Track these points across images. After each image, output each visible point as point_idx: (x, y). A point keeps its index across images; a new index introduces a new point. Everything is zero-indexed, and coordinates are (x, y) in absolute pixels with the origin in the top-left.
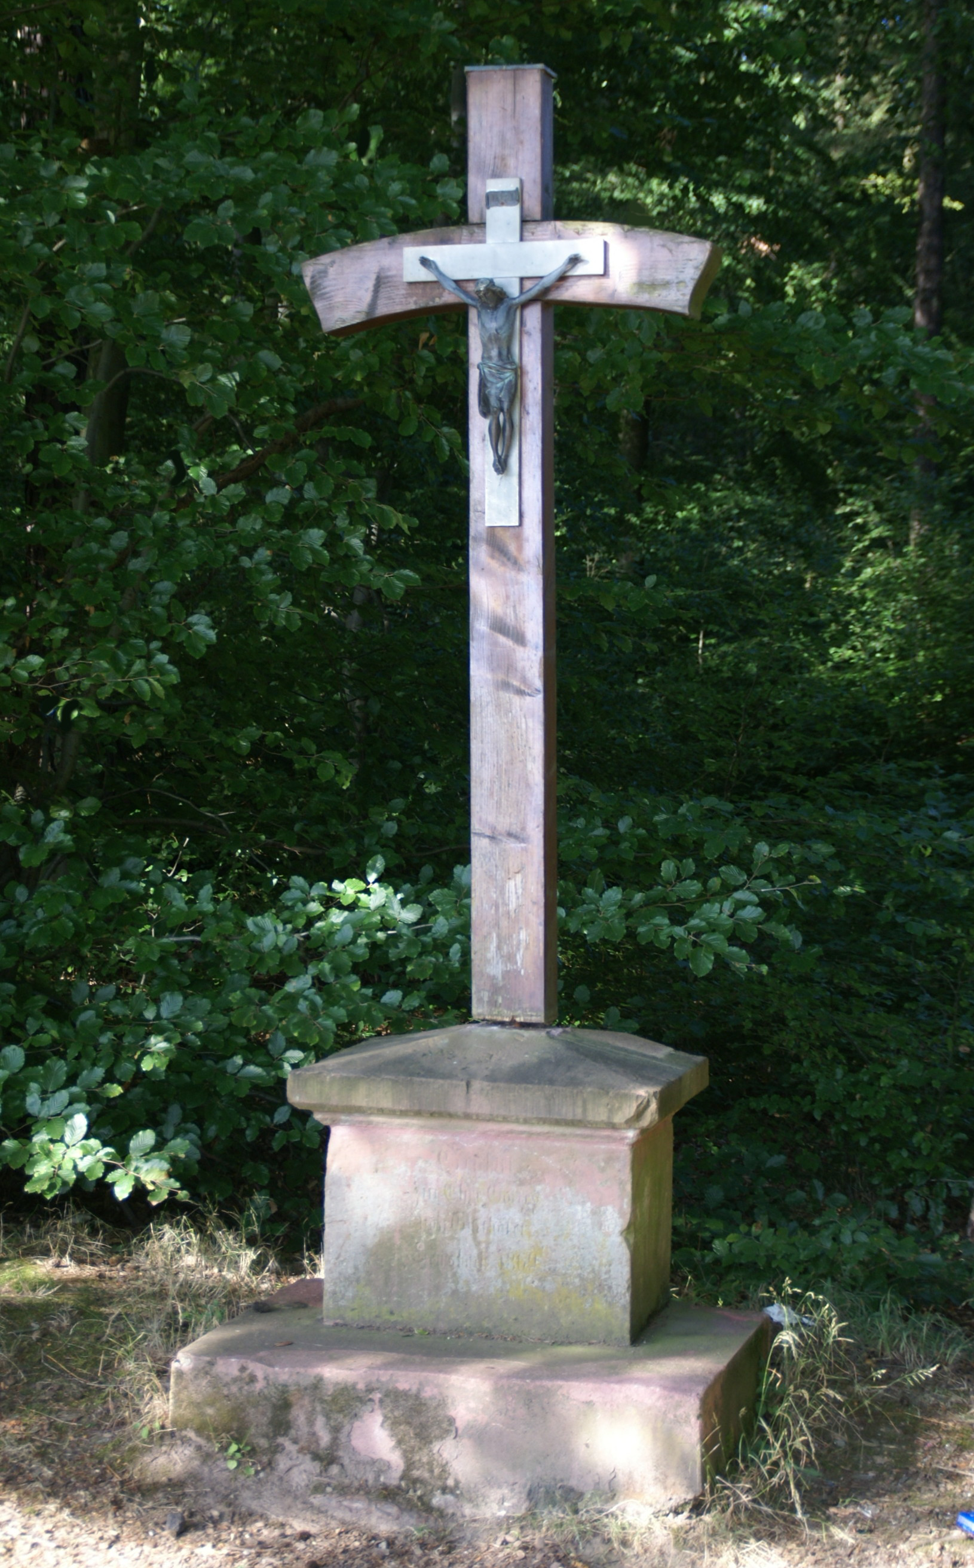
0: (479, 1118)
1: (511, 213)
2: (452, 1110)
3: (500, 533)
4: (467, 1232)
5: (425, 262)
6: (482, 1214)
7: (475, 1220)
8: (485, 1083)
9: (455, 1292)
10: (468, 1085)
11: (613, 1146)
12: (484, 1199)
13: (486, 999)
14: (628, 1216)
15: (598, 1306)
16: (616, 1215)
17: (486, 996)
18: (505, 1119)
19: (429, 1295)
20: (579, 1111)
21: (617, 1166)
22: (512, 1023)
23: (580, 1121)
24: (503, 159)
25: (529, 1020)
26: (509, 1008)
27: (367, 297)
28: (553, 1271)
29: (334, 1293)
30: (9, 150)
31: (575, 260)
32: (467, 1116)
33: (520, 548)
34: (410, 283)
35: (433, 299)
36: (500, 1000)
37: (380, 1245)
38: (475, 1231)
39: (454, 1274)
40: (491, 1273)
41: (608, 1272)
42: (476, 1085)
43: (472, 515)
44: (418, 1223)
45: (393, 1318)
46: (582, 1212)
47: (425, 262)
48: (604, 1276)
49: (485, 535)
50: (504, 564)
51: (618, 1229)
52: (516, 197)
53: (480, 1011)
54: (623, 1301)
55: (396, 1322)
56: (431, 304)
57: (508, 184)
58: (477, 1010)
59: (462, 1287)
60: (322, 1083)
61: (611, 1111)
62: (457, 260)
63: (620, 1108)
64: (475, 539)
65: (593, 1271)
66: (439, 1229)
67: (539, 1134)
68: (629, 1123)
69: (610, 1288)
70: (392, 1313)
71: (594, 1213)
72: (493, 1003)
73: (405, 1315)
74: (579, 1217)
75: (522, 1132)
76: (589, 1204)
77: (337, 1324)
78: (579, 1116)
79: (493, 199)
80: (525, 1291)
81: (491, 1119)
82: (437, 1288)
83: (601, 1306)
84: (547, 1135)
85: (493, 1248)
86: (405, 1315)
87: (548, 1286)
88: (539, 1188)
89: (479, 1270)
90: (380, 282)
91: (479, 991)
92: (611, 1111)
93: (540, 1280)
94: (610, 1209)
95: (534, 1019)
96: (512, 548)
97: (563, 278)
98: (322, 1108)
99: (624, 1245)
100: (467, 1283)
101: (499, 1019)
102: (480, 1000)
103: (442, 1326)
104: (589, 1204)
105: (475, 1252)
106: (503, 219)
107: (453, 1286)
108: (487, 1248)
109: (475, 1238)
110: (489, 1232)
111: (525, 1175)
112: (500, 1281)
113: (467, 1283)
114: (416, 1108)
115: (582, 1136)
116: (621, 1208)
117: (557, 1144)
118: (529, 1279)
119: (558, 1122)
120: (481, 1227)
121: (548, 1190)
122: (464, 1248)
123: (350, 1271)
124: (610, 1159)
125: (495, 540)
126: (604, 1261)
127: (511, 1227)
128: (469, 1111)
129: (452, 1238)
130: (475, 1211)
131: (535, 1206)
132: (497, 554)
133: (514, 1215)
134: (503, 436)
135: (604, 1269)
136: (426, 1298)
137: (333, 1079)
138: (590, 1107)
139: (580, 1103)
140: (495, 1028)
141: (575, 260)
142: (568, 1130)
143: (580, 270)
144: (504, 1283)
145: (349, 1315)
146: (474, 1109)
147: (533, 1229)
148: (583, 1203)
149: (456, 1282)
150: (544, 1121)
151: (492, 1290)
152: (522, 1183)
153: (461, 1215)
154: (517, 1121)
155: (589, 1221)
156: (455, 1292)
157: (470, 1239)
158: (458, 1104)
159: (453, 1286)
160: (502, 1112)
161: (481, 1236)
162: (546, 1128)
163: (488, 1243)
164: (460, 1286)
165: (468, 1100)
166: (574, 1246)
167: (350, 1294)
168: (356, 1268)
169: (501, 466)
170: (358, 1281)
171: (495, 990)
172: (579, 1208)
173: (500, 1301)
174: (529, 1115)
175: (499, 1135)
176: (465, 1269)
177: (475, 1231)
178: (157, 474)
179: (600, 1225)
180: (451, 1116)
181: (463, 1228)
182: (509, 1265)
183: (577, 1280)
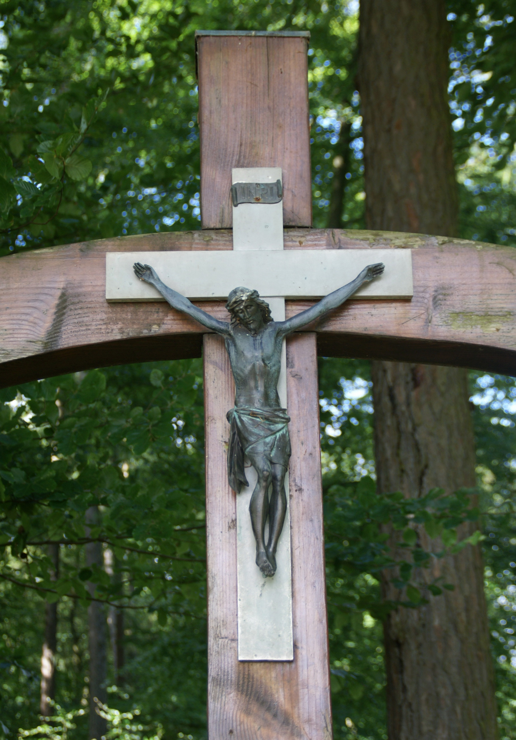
1: (272, 214)
3: (258, 671)
5: (142, 272)
24: (252, 145)
27: (46, 323)
30: (127, 736)
31: (375, 272)
33: (294, 698)
34: (114, 303)
35: (149, 326)
43: (213, 644)
47: (142, 272)
49: (233, 676)
50: (267, 724)
52: (273, 193)
56: (145, 333)
57: (266, 176)
62: (191, 273)
64: (218, 682)
79: (239, 194)
90: (64, 305)
96: (280, 697)
97: (351, 301)
106: (258, 224)
125: (249, 680)
132: (254, 707)
134: (269, 518)
141: (375, 272)
143: (376, 289)
169: (268, 567)
178: (466, 50)
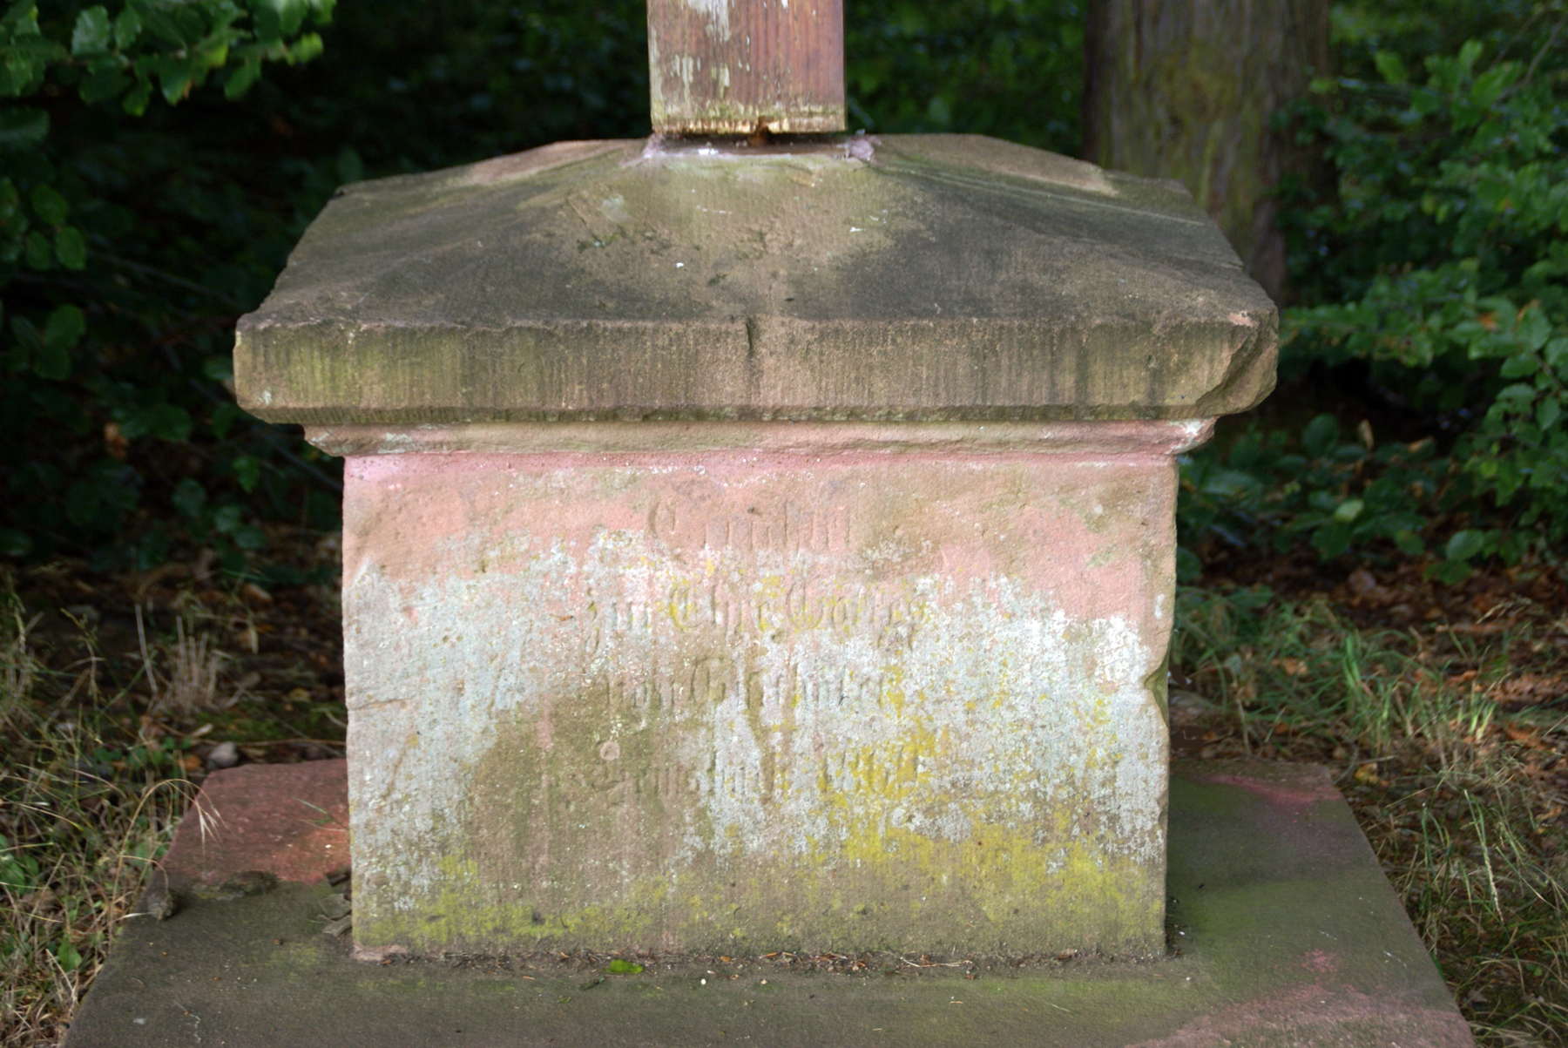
0: (778, 417)
2: (707, 401)
4: (734, 706)
6: (773, 657)
7: (752, 674)
8: (801, 324)
9: (704, 858)
10: (752, 331)
11: (1130, 462)
12: (778, 620)
13: (688, 78)
14: (1165, 638)
15: (1079, 866)
16: (1133, 637)
17: (686, 68)
18: (854, 416)
19: (636, 867)
20: (1068, 381)
21: (1139, 511)
22: (768, 140)
23: (1067, 409)
25: (803, 125)
26: (750, 98)
28: (963, 789)
29: (382, 881)
32: (748, 416)
36: (726, 80)
37: (499, 753)
38: (754, 702)
39: (701, 814)
40: (797, 805)
41: (1110, 780)
42: (775, 328)
44: (600, 694)
45: (539, 932)
46: (1039, 637)
48: (1099, 792)
51: (1140, 671)
53: (673, 110)
54: (1147, 850)
55: (548, 941)
58: (663, 109)
59: (721, 843)
60: (335, 350)
61: (1158, 377)
63: (1184, 366)
65: (1070, 781)
66: (656, 704)
67: (932, 445)
68: (1197, 411)
69: (1114, 819)
70: (537, 919)
71: (1072, 636)
72: (705, 87)
73: (573, 921)
74: (1032, 647)
75: (886, 444)
76: (1059, 615)
77: (392, 959)
78: (1068, 395)
80: (887, 841)
81: (818, 417)
82: (657, 851)
83: (1089, 866)
84: (951, 448)
85: (802, 742)
86: (573, 921)
87: (948, 826)
88: (924, 582)
89: (766, 800)
91: (666, 59)
92: (1158, 377)
93: (928, 812)
94: (1118, 622)
95: (818, 123)
98: (331, 417)
99: (1154, 710)
100: (736, 832)
101: (725, 128)
102: (672, 82)
103: (671, 941)
104: (1059, 615)
105: (756, 754)
107: (697, 842)
108: (787, 742)
109: (754, 721)
110: (791, 702)
111: (888, 552)
112: (822, 822)
113: (736, 832)
114: (607, 404)
115: (1053, 443)
116: (1148, 616)
117: (975, 466)
118: (899, 813)
119: (1001, 415)
120: (769, 692)
121: (950, 584)
122: (725, 752)
123: (423, 824)
124: (1117, 498)
126: (1100, 753)
127: (850, 688)
128: (755, 402)
129: (693, 724)
130: (754, 652)
131: (913, 629)
133: (861, 653)
135: (1098, 774)
136: (626, 876)
137: (366, 339)
138: (1098, 368)
139: (1069, 360)
140: (706, 152)
142: (1015, 432)
144: (832, 825)
145: (423, 932)
146: (771, 395)
147: (910, 688)
148: (1045, 613)
149: (707, 832)
150: (965, 415)
151: (802, 844)
152: (879, 573)
153: (714, 664)
154: (889, 419)
155: (1060, 657)
156: (704, 858)
157: (741, 723)
158: (725, 385)
159: (697, 842)
160: (850, 400)
161: (771, 715)
162: (955, 432)
163: (789, 731)
164: (715, 843)
165: (753, 372)
166: (1021, 723)
167: (422, 881)
168: (438, 816)
170: (443, 847)
171: (709, 52)
172: (1034, 625)
173: (822, 871)
174: (926, 402)
175: (821, 452)
176: (729, 797)
177: (754, 702)
179: (1091, 665)
180: (700, 416)
181: (721, 698)
182: (845, 781)
183: (1026, 807)
